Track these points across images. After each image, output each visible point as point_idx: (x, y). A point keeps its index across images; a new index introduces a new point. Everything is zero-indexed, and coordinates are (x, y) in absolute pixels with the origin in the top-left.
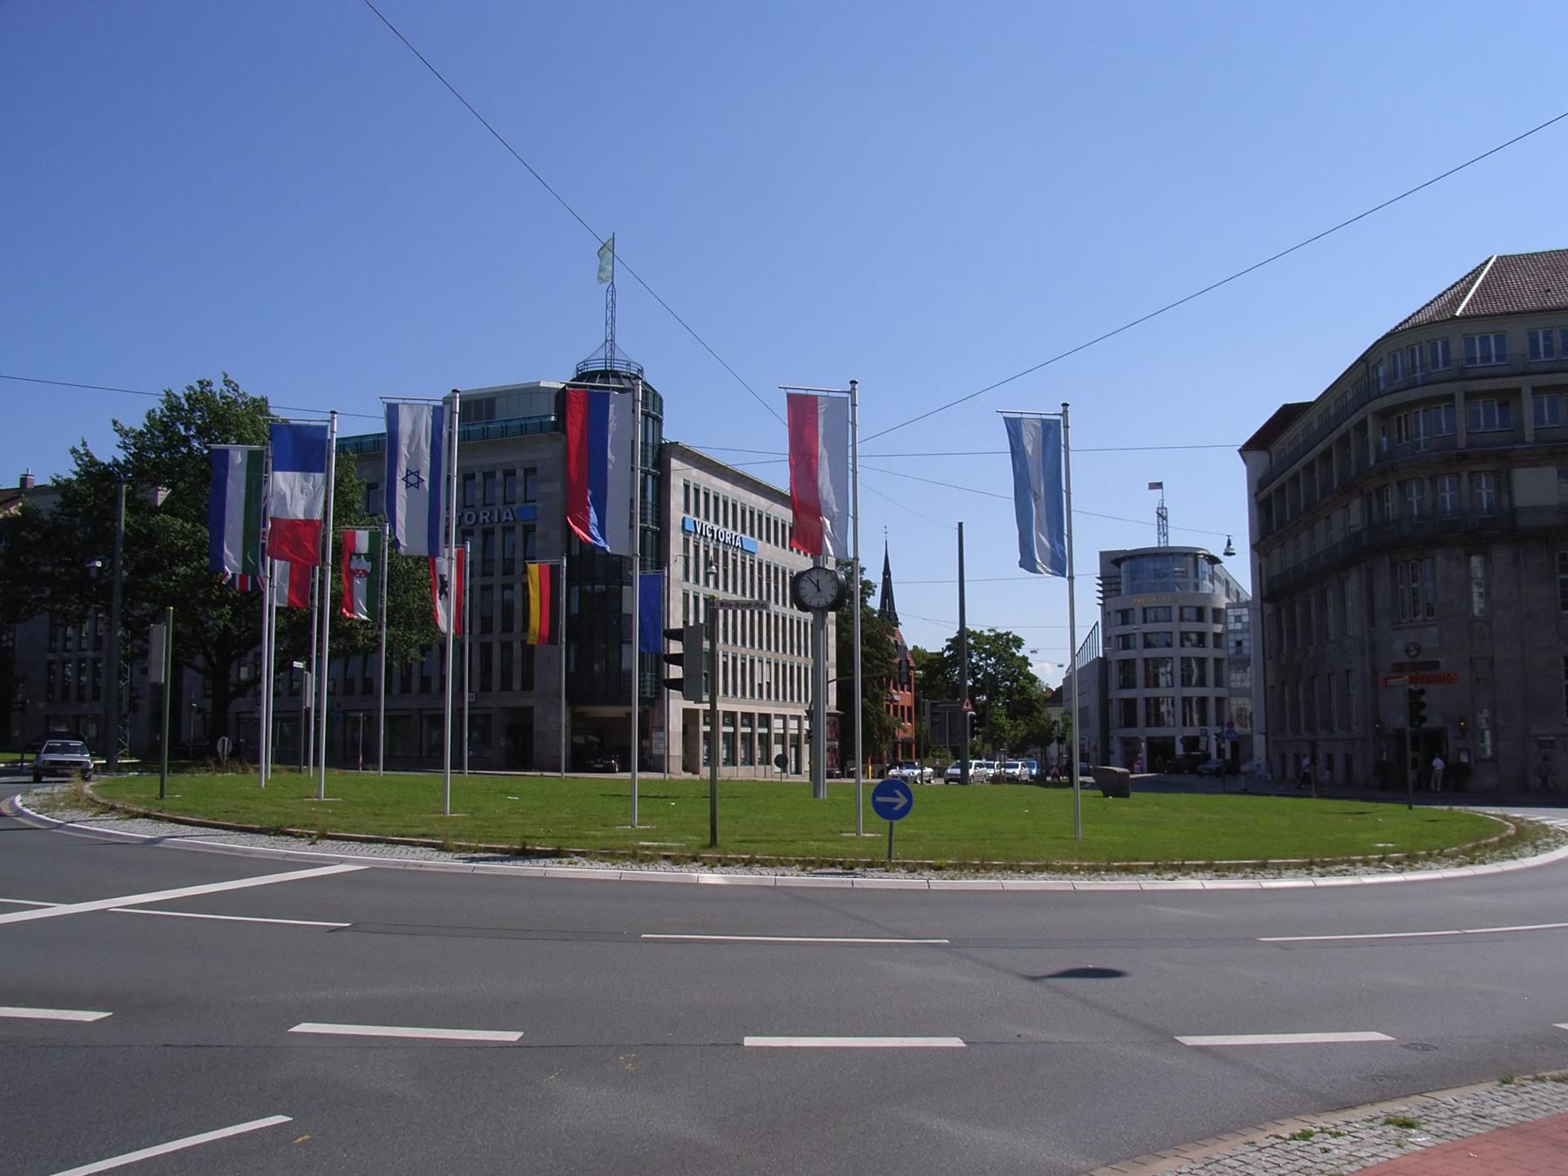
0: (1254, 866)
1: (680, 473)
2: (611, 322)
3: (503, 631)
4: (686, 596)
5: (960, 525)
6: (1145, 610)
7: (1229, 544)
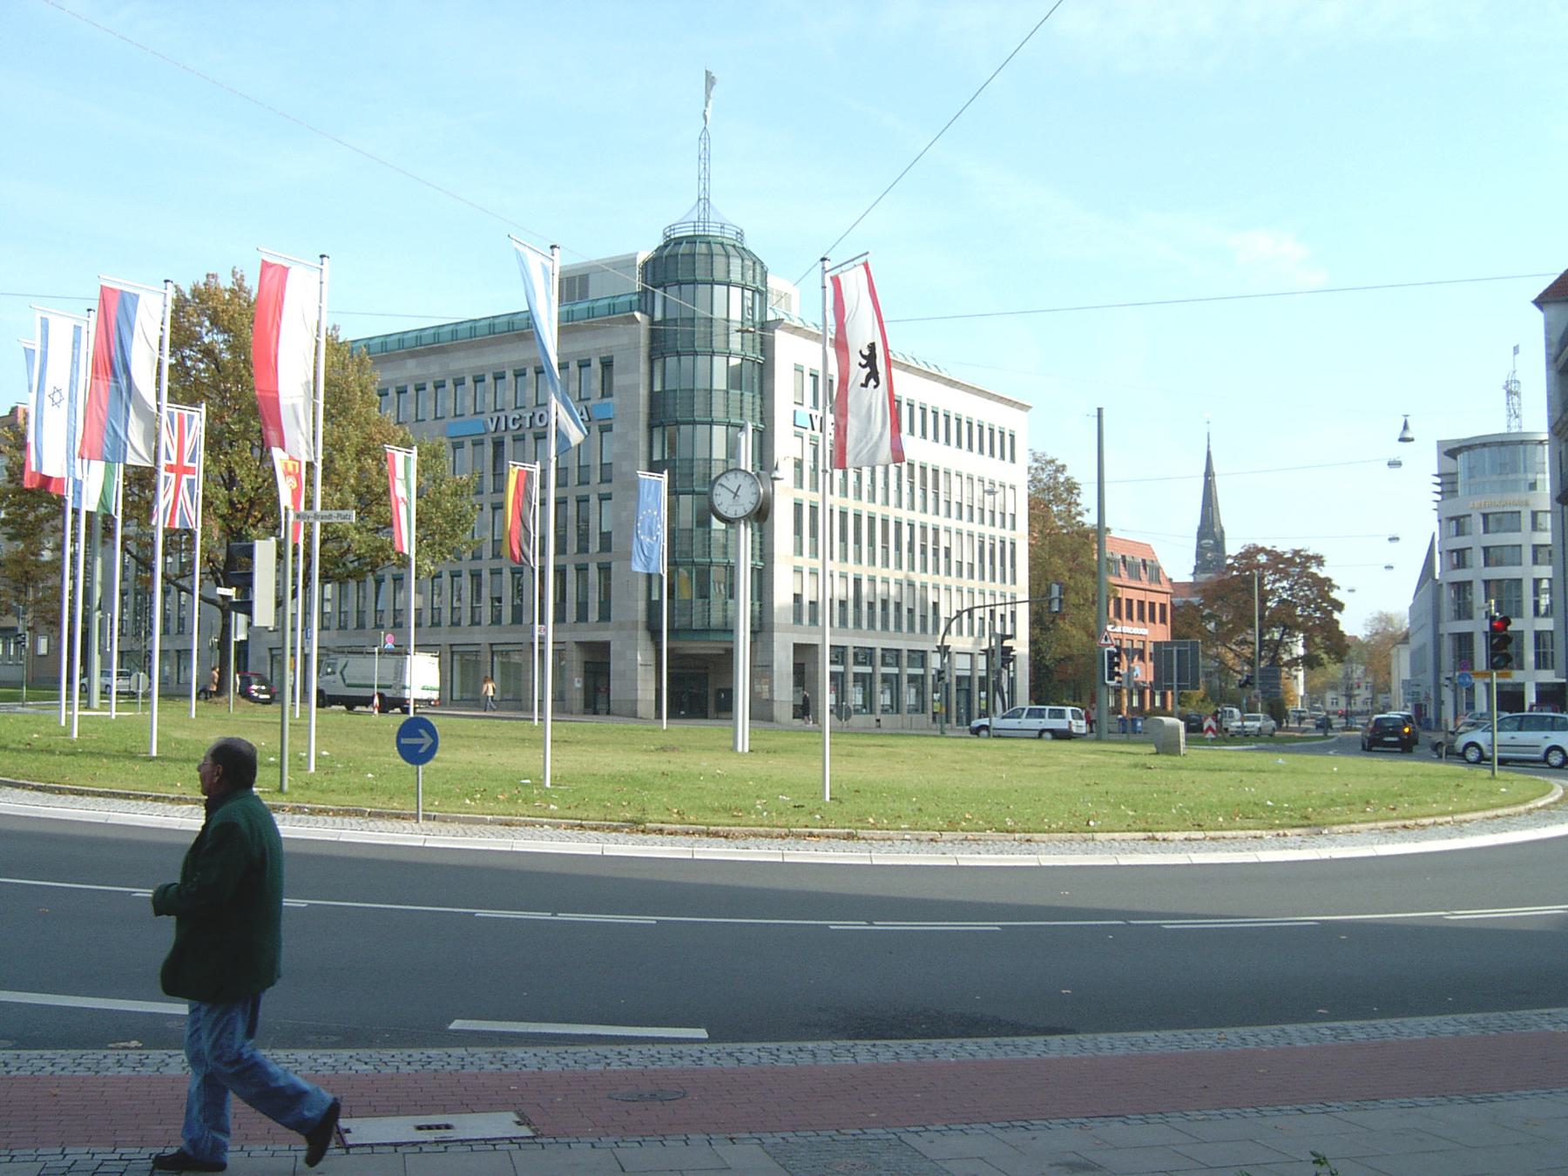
2: (704, 177)
3: (602, 550)
5: (1100, 410)
6: (1485, 516)
7: (1406, 427)
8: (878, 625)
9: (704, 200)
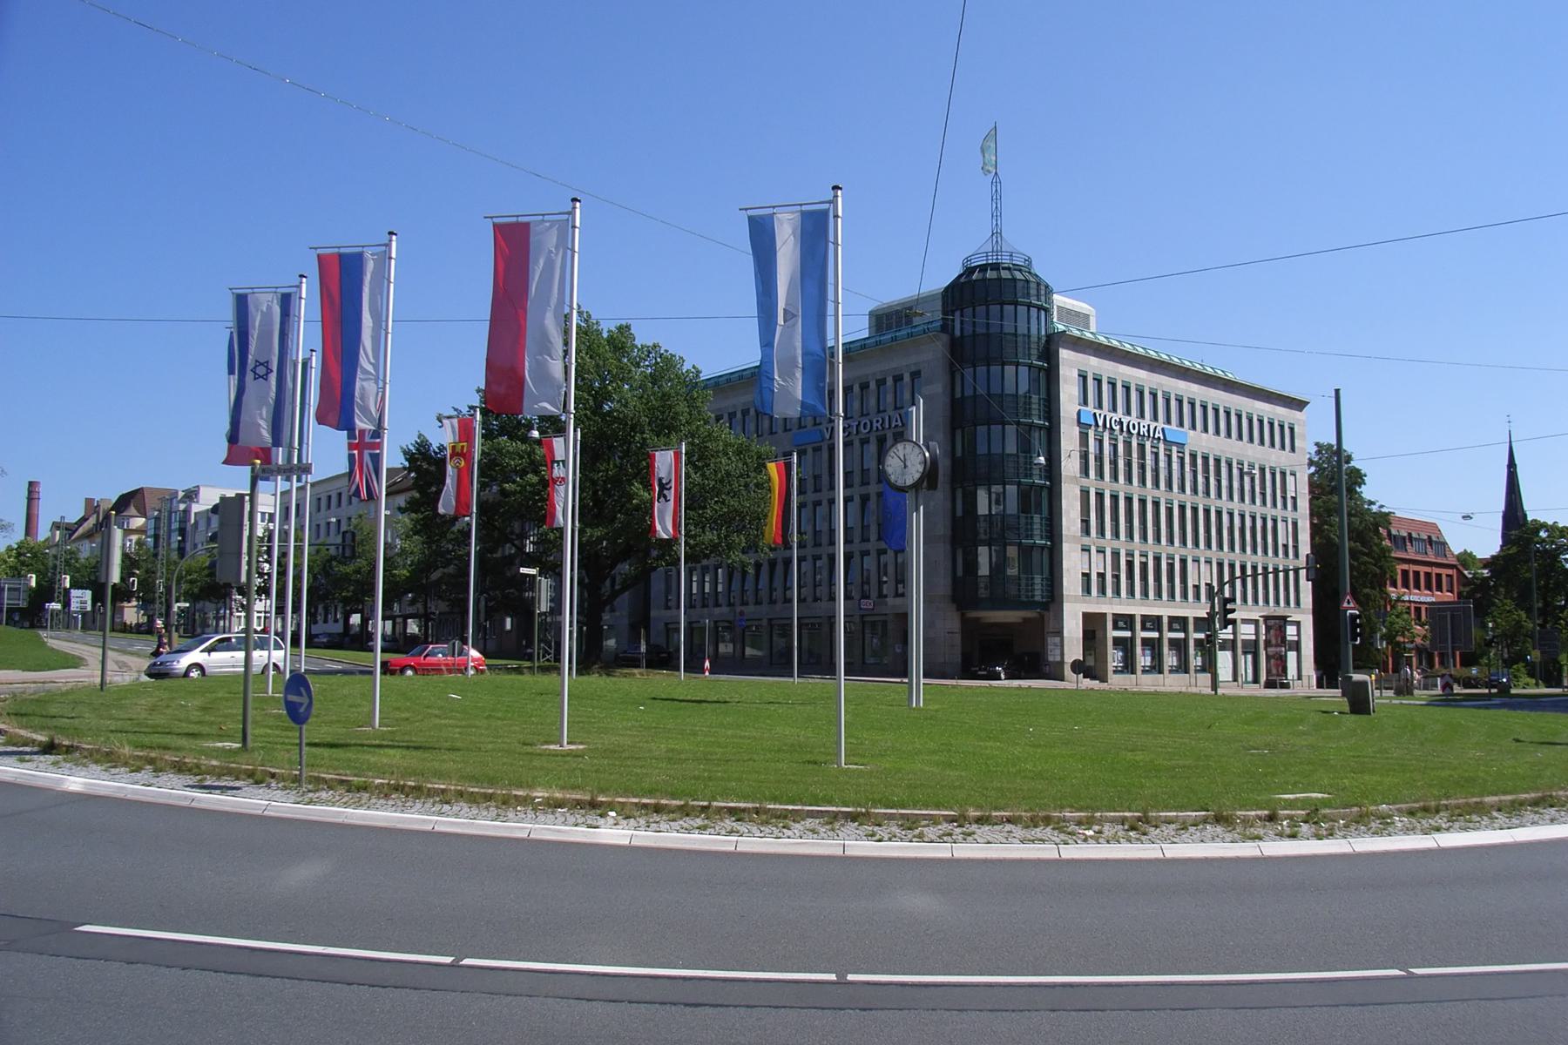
0: (579, 804)
1: (1070, 363)
2: (996, 214)
4: (1085, 493)
5: (1337, 391)
8: (1261, 602)
9: (996, 234)
